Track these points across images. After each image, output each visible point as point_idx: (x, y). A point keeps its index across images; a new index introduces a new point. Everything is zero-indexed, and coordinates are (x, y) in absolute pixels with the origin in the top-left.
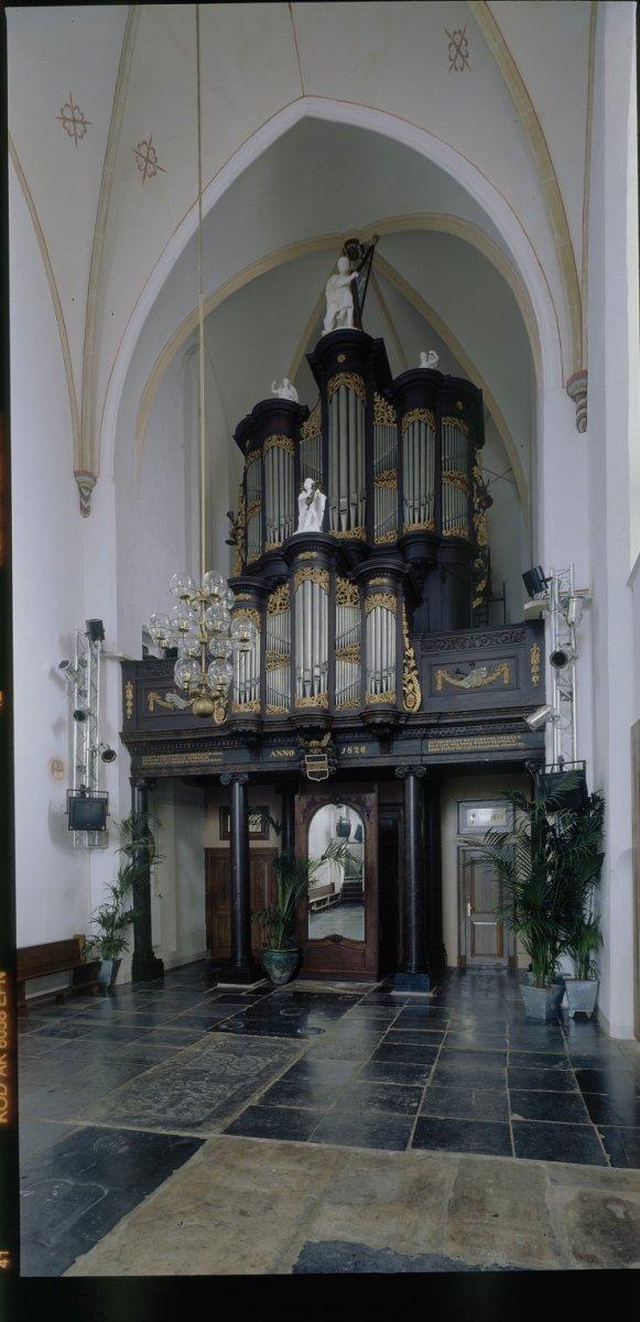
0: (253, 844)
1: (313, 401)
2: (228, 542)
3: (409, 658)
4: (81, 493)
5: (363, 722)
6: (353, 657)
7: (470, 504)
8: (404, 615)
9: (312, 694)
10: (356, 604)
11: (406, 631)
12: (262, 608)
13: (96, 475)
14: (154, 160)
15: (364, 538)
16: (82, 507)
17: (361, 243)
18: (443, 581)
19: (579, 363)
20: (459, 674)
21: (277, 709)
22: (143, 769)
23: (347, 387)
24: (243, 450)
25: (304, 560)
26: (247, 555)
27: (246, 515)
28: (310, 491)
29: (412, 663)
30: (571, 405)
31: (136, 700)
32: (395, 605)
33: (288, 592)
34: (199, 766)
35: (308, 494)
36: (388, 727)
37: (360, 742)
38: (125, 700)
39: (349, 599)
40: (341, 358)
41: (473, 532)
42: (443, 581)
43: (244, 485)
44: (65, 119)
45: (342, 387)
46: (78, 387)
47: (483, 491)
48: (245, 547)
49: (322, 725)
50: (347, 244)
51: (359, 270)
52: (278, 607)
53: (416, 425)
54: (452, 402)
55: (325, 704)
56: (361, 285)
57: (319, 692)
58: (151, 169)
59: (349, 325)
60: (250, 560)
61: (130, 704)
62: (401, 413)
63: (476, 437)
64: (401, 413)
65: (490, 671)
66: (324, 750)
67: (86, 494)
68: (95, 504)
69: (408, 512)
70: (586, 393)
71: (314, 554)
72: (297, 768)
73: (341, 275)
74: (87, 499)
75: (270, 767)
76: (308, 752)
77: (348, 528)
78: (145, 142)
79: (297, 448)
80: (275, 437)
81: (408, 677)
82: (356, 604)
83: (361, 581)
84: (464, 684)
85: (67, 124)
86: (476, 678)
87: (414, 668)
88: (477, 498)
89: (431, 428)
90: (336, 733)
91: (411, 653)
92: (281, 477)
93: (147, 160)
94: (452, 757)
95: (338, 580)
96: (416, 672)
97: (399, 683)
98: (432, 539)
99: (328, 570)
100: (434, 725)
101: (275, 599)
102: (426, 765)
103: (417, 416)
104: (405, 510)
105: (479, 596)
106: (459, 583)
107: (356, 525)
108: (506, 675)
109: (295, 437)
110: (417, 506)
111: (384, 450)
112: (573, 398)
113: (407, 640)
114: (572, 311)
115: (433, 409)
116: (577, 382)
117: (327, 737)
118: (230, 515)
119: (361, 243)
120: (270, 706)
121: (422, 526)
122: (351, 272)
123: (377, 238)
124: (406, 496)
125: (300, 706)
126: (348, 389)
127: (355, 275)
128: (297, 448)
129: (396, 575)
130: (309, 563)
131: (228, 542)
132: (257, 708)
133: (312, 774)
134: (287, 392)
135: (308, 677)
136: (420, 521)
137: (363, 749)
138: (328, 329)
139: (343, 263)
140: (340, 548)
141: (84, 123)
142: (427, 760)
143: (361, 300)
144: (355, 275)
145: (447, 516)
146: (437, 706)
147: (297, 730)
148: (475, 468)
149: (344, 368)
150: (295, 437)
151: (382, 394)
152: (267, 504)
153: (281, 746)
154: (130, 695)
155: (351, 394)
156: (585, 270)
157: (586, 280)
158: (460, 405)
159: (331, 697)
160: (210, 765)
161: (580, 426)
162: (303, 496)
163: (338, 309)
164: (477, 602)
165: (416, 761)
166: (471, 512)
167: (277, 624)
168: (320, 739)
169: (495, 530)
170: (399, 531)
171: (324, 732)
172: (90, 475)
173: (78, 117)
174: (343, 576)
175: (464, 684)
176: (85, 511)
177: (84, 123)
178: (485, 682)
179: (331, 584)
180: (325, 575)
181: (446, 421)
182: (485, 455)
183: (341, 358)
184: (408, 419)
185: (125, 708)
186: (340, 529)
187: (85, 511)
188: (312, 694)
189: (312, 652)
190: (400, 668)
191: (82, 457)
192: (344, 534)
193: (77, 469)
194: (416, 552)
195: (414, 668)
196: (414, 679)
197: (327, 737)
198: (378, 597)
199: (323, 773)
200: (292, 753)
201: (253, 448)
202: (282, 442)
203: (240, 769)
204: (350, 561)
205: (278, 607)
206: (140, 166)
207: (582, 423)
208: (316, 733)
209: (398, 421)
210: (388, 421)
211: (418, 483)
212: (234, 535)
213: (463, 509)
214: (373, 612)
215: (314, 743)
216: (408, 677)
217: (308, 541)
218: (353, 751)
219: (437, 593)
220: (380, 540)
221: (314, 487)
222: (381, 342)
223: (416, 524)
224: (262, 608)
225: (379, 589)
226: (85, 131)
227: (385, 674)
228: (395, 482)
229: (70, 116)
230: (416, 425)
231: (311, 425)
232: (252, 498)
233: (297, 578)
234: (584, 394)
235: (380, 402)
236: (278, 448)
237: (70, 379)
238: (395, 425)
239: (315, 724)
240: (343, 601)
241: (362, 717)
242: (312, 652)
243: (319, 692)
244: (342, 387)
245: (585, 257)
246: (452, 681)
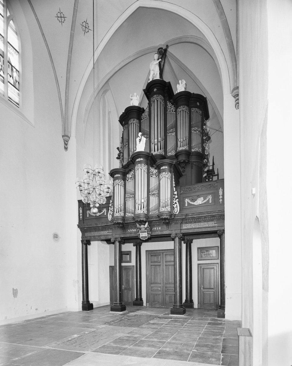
0: (123, 264)
1: (145, 106)
2: (117, 158)
3: (175, 195)
4: (65, 143)
5: (159, 218)
6: (155, 195)
7: (202, 140)
8: (174, 180)
9: (141, 209)
10: (157, 176)
11: (174, 185)
12: (124, 179)
13: (70, 136)
14: (88, 27)
15: (163, 154)
16: (65, 148)
17: (163, 49)
18: (192, 168)
19: (236, 84)
20: (193, 200)
21: (130, 215)
22: (86, 237)
23: (158, 99)
24: (122, 125)
25: (138, 161)
26: (123, 162)
27: (123, 148)
28: (140, 137)
29: (176, 197)
30: (234, 99)
31: (83, 213)
32: (170, 176)
33: (133, 173)
34: (104, 235)
35: (140, 138)
36: (168, 220)
37: (158, 225)
38: (79, 214)
39: (154, 175)
40: (155, 90)
41: (203, 149)
42: (192, 168)
43: (123, 138)
44: (58, 17)
45: (156, 100)
46: (64, 107)
47: (207, 134)
48: (123, 159)
49: (144, 219)
50: (159, 49)
51: (161, 58)
52: (130, 179)
53: (182, 112)
54: (197, 104)
55: (146, 212)
56: (162, 64)
57: (144, 208)
58: (87, 30)
59: (158, 77)
60: (124, 164)
61: (81, 215)
62: (177, 107)
63: (206, 116)
64: (177, 107)
65: (205, 199)
66: (146, 229)
67: (66, 143)
68: (69, 146)
69: (179, 143)
70: (238, 94)
71: (142, 159)
72: (137, 236)
73: (156, 61)
74: (67, 145)
75: (128, 235)
76: (140, 229)
77: (158, 150)
78: (84, 22)
79: (140, 123)
80: (132, 119)
81: (175, 202)
82: (157, 176)
83: (158, 168)
84: (196, 203)
85: (59, 18)
86: (200, 201)
87: (177, 198)
88: (205, 137)
89: (187, 112)
90: (150, 223)
91: (176, 193)
92: (135, 133)
93: (86, 27)
94: (191, 230)
95: (151, 168)
96: (177, 200)
97: (172, 204)
98: (188, 153)
99: (147, 165)
100: (185, 220)
101: (129, 176)
102: (182, 233)
103: (182, 109)
104: (179, 141)
105: (205, 173)
106: (196, 169)
107: (161, 149)
108: (210, 200)
109: (139, 119)
110: (182, 141)
111: (171, 122)
112: (234, 97)
113: (174, 188)
114: (233, 65)
115: (188, 106)
116: (235, 91)
117: (147, 223)
118: (118, 148)
119: (163, 49)
120: (127, 214)
121: (184, 148)
122: (158, 59)
123: (167, 46)
124: (178, 138)
125: (137, 213)
126: (157, 101)
127: (160, 60)
128: (140, 123)
129: (170, 165)
130: (140, 162)
131: (117, 158)
132: (122, 214)
133: (142, 237)
134: (135, 102)
135: (140, 203)
136: (183, 146)
137: (160, 228)
138: (151, 80)
139: (156, 56)
140: (151, 156)
141: (64, 17)
142: (183, 231)
143: (162, 67)
144: (160, 60)
145: (193, 145)
146: (185, 212)
147: (136, 221)
148: (204, 127)
149: (155, 93)
150: (139, 119)
151: (170, 102)
152: (130, 141)
153: (132, 228)
154: (81, 211)
155: (159, 102)
156: (237, 50)
157: (238, 54)
158: (198, 104)
159: (148, 210)
160: (107, 235)
161: (237, 107)
162: (138, 139)
163: (155, 74)
164: (205, 175)
165: (178, 232)
166: (203, 142)
167: (130, 185)
168: (144, 225)
169: (211, 148)
170: (176, 151)
171: (145, 222)
172: (67, 136)
173: (62, 16)
174: (152, 166)
175: (196, 203)
176: (66, 149)
177: (64, 17)
178: (203, 202)
179: (148, 170)
180: (146, 167)
181: (193, 110)
182: (208, 123)
183: (155, 90)
184: (179, 110)
185: (79, 216)
186: (155, 151)
187: (66, 149)
188: (141, 209)
189: (141, 195)
190: (172, 198)
191: (65, 131)
192: (156, 153)
193: (63, 134)
194: (182, 158)
195: (177, 198)
196: (177, 203)
197: (147, 223)
198: (164, 173)
199: (145, 237)
200: (135, 230)
201: (125, 124)
202: (135, 121)
203: (117, 236)
204: (152, 161)
205: (130, 179)
206: (83, 29)
207: (237, 105)
208: (142, 222)
209: (176, 111)
210: (172, 111)
211: (182, 134)
212: (119, 155)
213: (200, 141)
214: (162, 179)
215: (142, 226)
216: (175, 202)
217: (139, 154)
218: (156, 229)
219: (190, 173)
220: (169, 154)
221: (142, 135)
222: (169, 83)
223: (182, 148)
224: (124, 179)
225: (164, 170)
226: (65, 20)
227: (166, 201)
228: (175, 133)
229: (60, 16)
230: (182, 112)
231: (145, 115)
232: (126, 141)
233: (136, 167)
234: (238, 95)
235: (169, 105)
236: (133, 123)
237: (61, 104)
238: (175, 113)
239: (142, 219)
240: (152, 175)
241: (158, 216)
242: (141, 195)
243: (144, 208)
244: (156, 100)
245: (237, 46)
246: (191, 203)
